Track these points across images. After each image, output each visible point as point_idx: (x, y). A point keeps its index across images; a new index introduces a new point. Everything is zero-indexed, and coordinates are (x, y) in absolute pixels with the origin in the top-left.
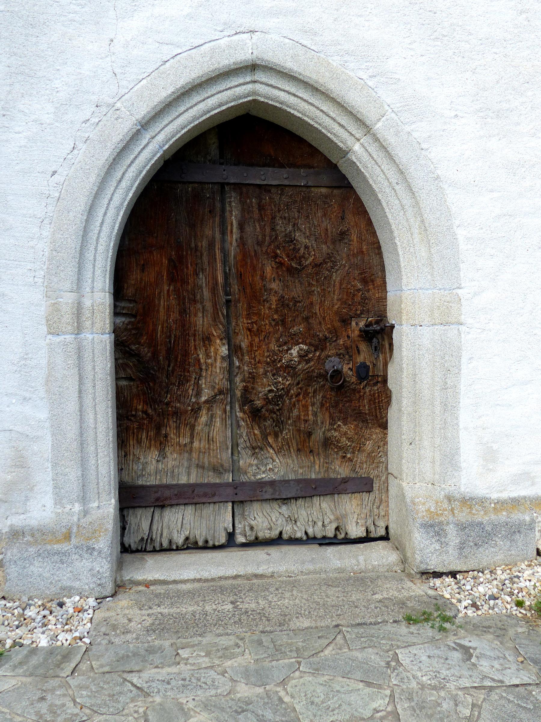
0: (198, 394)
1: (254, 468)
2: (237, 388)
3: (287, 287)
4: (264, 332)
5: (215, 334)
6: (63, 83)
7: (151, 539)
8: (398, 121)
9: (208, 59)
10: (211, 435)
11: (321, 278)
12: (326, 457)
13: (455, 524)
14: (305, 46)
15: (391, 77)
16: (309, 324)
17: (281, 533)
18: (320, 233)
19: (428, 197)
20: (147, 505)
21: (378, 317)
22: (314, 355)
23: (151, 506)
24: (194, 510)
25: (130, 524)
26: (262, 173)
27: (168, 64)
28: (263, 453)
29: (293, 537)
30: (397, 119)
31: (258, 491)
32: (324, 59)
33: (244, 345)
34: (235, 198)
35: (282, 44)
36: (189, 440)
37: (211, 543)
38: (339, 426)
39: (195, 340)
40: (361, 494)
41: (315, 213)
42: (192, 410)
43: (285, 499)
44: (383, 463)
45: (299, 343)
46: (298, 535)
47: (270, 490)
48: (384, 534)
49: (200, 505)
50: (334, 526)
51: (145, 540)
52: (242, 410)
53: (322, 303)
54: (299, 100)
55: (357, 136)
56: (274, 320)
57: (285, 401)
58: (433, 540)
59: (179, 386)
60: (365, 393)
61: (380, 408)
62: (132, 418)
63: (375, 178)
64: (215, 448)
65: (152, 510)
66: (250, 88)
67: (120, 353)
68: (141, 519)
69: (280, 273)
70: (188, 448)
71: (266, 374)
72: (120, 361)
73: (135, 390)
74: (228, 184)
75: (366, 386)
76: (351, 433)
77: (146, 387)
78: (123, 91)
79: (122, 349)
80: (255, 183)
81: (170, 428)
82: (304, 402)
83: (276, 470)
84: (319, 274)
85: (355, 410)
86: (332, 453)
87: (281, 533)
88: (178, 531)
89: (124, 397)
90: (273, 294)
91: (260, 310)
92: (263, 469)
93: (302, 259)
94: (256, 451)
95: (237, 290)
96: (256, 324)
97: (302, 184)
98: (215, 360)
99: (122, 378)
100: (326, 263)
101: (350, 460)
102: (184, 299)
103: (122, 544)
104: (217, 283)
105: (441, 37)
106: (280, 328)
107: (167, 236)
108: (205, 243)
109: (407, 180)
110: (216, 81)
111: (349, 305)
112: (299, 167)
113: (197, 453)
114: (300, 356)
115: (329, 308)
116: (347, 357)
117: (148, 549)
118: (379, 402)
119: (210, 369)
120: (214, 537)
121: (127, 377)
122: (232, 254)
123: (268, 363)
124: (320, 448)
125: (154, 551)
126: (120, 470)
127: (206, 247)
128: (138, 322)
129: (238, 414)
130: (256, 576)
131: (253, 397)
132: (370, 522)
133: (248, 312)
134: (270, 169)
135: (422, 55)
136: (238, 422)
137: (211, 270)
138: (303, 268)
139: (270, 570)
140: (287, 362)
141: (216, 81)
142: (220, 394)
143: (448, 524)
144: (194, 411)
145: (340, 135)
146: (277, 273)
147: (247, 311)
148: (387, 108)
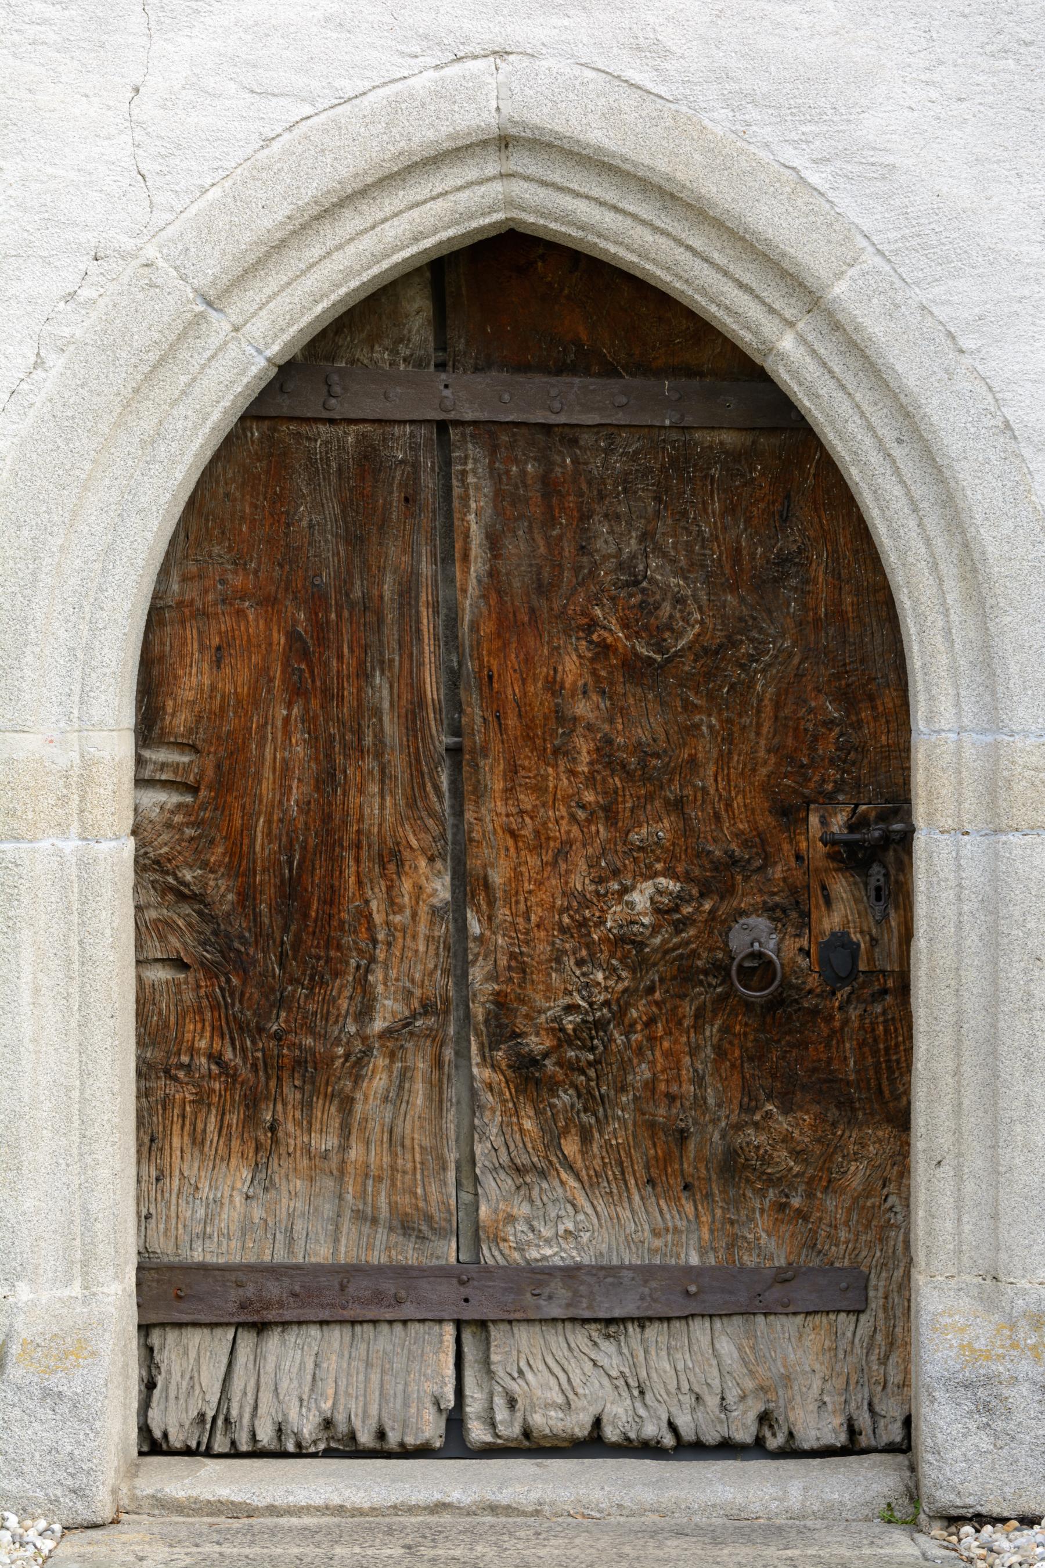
0: (365, 1012)
1: (522, 1226)
2: (475, 995)
3: (623, 711)
4: (555, 839)
5: (414, 843)
6: (12, 202)
7: (227, 1420)
8: (895, 279)
9: (380, 127)
10: (398, 1130)
11: (721, 687)
12: (738, 1202)
13: (1035, 1383)
14: (638, 87)
15: (872, 160)
16: (686, 819)
17: (597, 1423)
18: (719, 559)
19: (977, 481)
20: (215, 1320)
21: (887, 802)
22: (697, 910)
23: (228, 1324)
24: (347, 1338)
25: (169, 1372)
26: (553, 392)
27: (276, 146)
28: (545, 1185)
29: (632, 1435)
30: (892, 273)
31: (529, 1295)
32: (689, 119)
33: (497, 877)
34: (476, 461)
35: (577, 83)
36: (336, 1142)
37: (393, 1439)
38: (768, 1115)
39: (358, 861)
40: (832, 1317)
41: (704, 503)
42: (347, 1056)
43: (609, 1322)
44: (899, 1227)
45: (656, 874)
46: (650, 1430)
47: (563, 1294)
48: (898, 1439)
49: (365, 1326)
50: (756, 1407)
51: (209, 1420)
52: (486, 1060)
53: (723, 760)
54: (629, 221)
55: (788, 313)
56: (583, 807)
57: (611, 1040)
58: (972, 1426)
59: (312, 989)
60: (846, 1022)
61: (889, 1068)
62: (181, 1074)
63: (839, 425)
64: (409, 1166)
65: (230, 1335)
66: (498, 193)
67: (152, 892)
68: (198, 1360)
69: (603, 673)
70: (334, 1162)
71: (558, 961)
72: (152, 914)
73: (189, 997)
74: (458, 423)
75: (849, 1001)
76: (803, 1137)
77: (222, 989)
78: (161, 217)
79: (157, 881)
80: (532, 419)
81: (285, 1104)
82: (666, 1044)
83: (585, 1237)
84: (715, 676)
85: (815, 1070)
86: (749, 1194)
87: (597, 1423)
88: (301, 1400)
89: (160, 1014)
90: (580, 730)
91: (545, 778)
92: (547, 1232)
93: (667, 635)
94: (528, 1179)
95: (478, 720)
96: (532, 818)
97: (667, 422)
98: (414, 915)
99: (157, 960)
100: (735, 645)
101: (802, 1215)
102: (331, 739)
103: (145, 1430)
104: (420, 702)
105: (1013, 46)
106: (601, 829)
107: (287, 567)
108: (388, 588)
109: (921, 436)
110: (404, 180)
111: (802, 766)
112: (659, 373)
113: (359, 1180)
114: (657, 910)
115: (742, 773)
116: (794, 915)
117: (217, 1448)
118: (887, 1049)
119: (400, 940)
120: (405, 1425)
121: (169, 959)
122: (467, 618)
123: (563, 930)
124: (714, 1177)
125: (235, 1454)
126: (145, 1218)
127: (392, 600)
128: (203, 807)
129: (475, 1071)
130: (493, 1509)
131: (521, 1024)
132: (859, 1397)
133: (509, 785)
134: (577, 380)
135: (960, 99)
136: (473, 1093)
137: (406, 666)
138: (668, 661)
139: (534, 1496)
140: (621, 926)
141: (404, 180)
142: (426, 1014)
143: (1014, 1380)
144: (353, 1059)
145: (741, 311)
146: (594, 673)
147: (505, 780)
148: (863, 243)
